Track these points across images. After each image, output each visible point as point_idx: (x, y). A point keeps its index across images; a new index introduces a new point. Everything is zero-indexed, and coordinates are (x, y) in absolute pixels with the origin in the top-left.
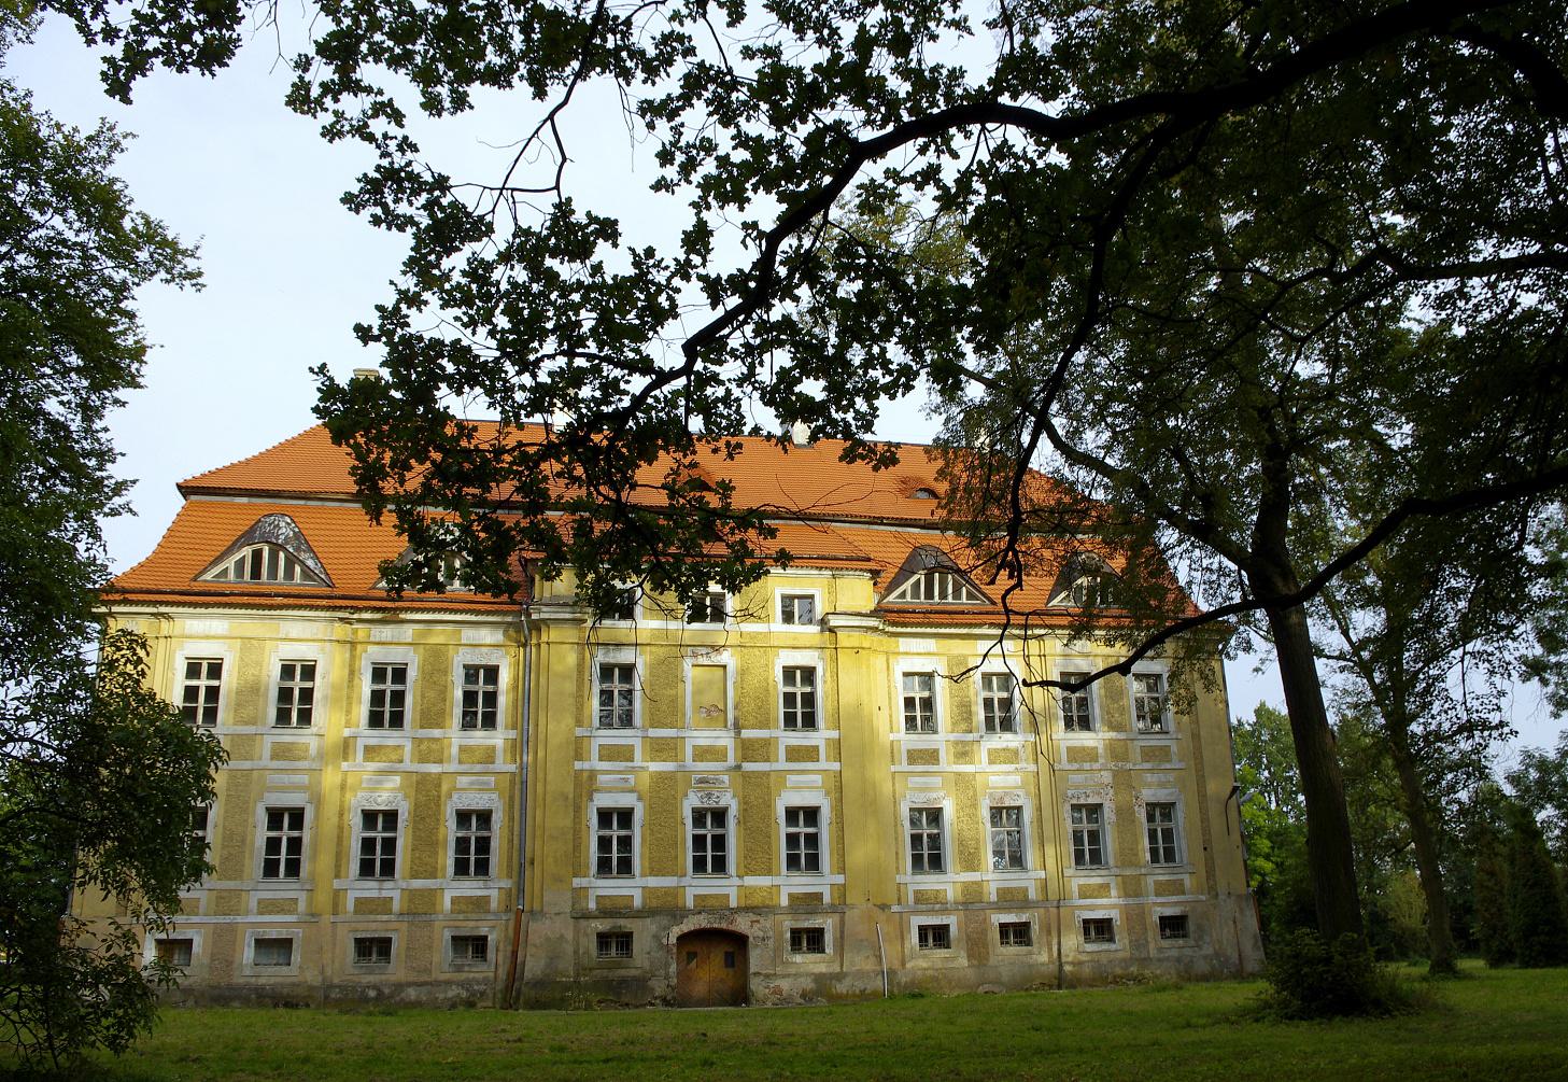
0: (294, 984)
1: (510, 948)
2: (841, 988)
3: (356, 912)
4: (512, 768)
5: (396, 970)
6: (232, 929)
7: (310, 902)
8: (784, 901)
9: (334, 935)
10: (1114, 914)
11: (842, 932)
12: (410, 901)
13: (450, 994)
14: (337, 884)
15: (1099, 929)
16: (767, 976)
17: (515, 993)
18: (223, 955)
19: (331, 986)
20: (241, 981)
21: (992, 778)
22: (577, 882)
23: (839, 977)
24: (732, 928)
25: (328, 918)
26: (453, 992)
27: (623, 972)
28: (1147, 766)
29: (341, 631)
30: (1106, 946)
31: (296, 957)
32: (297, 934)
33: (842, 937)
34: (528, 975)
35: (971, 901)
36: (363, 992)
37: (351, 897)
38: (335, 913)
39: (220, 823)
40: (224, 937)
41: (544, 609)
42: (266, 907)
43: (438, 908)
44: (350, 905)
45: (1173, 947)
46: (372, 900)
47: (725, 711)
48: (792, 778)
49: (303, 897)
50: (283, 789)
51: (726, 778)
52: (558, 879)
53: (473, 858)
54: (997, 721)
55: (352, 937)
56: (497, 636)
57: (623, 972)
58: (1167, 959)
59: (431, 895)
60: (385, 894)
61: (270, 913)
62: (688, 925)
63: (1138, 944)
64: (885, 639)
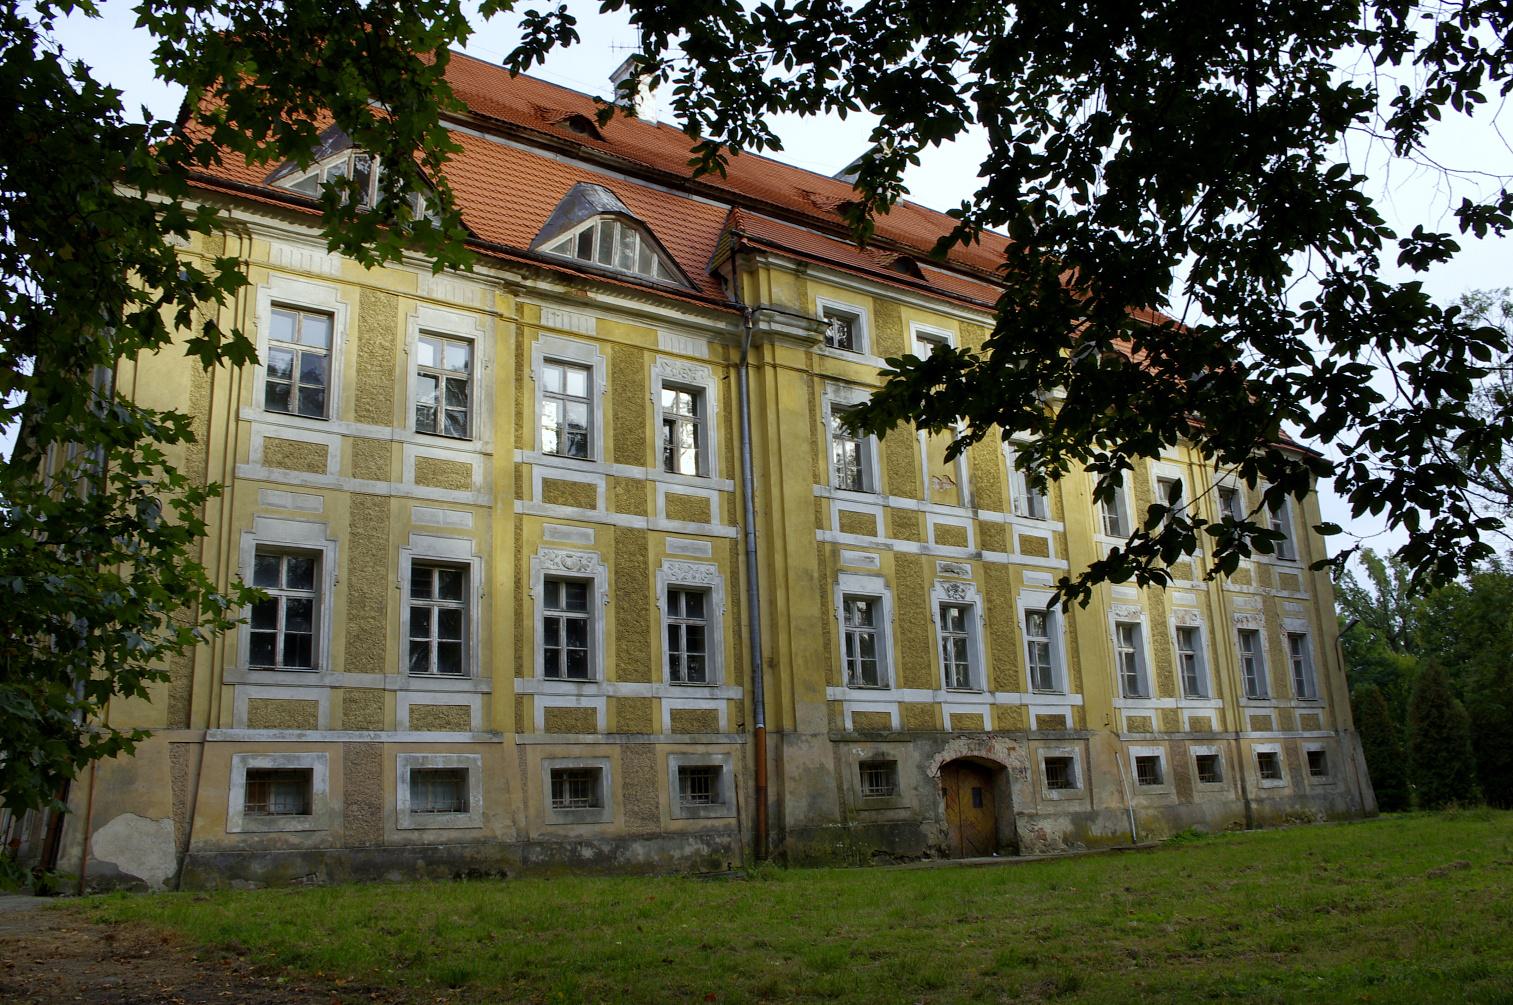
0: (477, 842)
1: (751, 783)
2: (1096, 830)
3: (548, 729)
4: (731, 532)
5: (613, 819)
6: (373, 752)
7: (488, 710)
9: (523, 762)
11: (1088, 763)
12: (619, 713)
13: (688, 851)
14: (519, 686)
16: (1031, 817)
17: (770, 843)
18: (362, 799)
19: (529, 844)
20: (397, 837)
22: (832, 692)
23: (1092, 816)
24: (992, 756)
25: (510, 738)
26: (691, 848)
27: (891, 814)
28: (1285, 593)
29: (504, 303)
31: (476, 798)
32: (474, 761)
33: (1089, 769)
34: (789, 821)
36: (574, 851)
37: (540, 704)
38: (519, 730)
39: (344, 575)
40: (362, 764)
41: (778, 317)
42: (426, 718)
43: (656, 726)
44: (540, 720)
46: (567, 711)
47: (957, 484)
49: (476, 703)
51: (968, 567)
52: (811, 688)
53: (690, 656)
54: (564, 658)
55: (548, 766)
56: (699, 347)
57: (891, 814)
59: (646, 704)
60: (585, 703)
61: (430, 727)
62: (949, 754)
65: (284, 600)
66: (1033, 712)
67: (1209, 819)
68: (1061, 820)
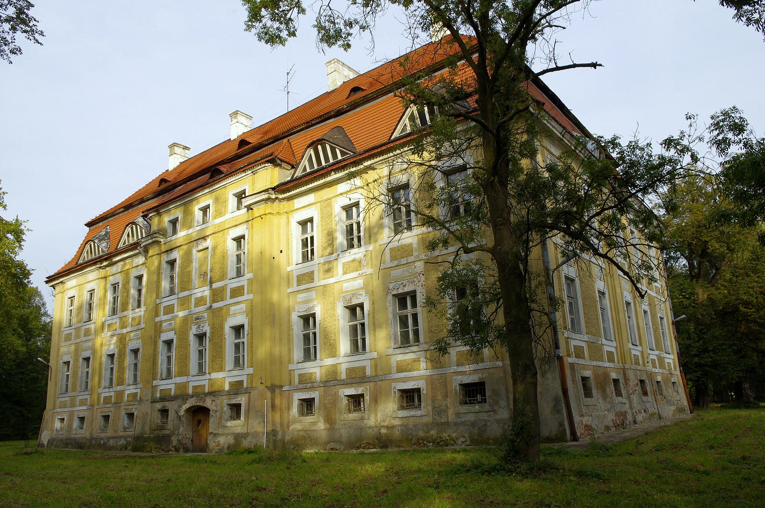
8: (227, 388)
10: (421, 384)
11: (249, 406)
15: (410, 397)
16: (215, 435)
21: (345, 285)
24: (205, 405)
30: (412, 412)
35: (332, 380)
45: (472, 412)
48: (233, 308)
50: (404, 380)
58: (463, 423)
63: (439, 411)
64: (285, 203)
65: (358, 325)
66: (191, 384)
67: (344, 439)
68: (229, 437)
